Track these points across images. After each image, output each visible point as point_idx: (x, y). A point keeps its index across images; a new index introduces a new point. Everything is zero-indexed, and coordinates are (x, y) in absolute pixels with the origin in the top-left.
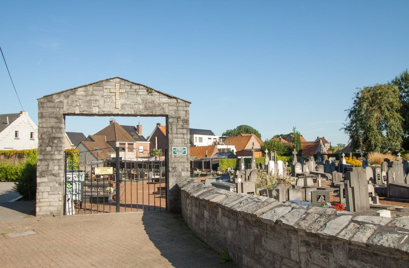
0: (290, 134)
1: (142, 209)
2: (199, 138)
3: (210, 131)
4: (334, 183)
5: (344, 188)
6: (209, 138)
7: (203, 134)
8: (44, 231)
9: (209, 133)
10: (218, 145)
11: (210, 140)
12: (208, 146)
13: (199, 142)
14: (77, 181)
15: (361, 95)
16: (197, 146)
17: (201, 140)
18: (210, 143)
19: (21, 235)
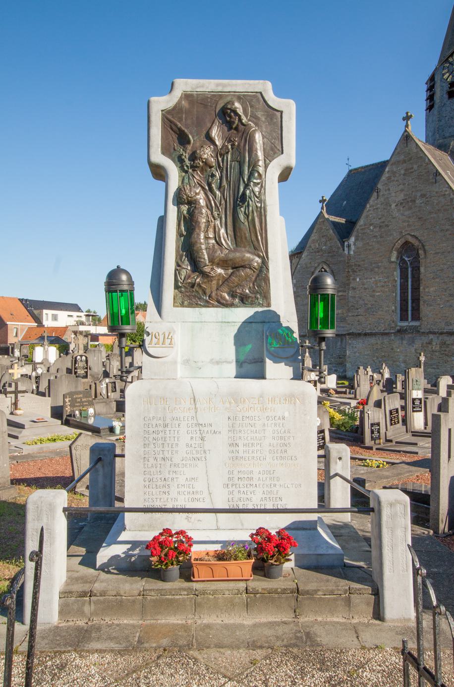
0: (232, 305)
1: (90, 505)
2: (53, 315)
3: (76, 305)
4: (403, 425)
5: (88, 484)
6: (69, 316)
7: (61, 310)
8: (366, 577)
9: (75, 308)
10: (80, 326)
11: (70, 318)
12: (421, 316)
13: (52, 320)
14: (16, 387)
15: (239, 261)
16: (46, 326)
17: (55, 318)
18: (71, 322)
19: (116, 622)
